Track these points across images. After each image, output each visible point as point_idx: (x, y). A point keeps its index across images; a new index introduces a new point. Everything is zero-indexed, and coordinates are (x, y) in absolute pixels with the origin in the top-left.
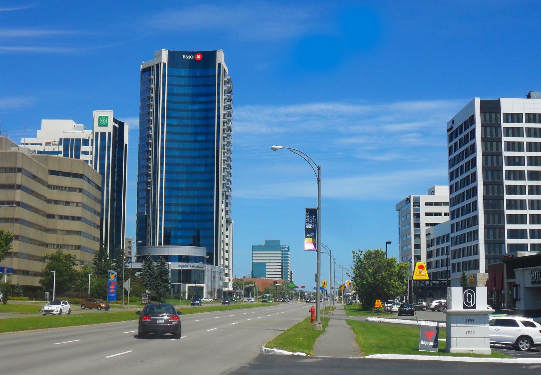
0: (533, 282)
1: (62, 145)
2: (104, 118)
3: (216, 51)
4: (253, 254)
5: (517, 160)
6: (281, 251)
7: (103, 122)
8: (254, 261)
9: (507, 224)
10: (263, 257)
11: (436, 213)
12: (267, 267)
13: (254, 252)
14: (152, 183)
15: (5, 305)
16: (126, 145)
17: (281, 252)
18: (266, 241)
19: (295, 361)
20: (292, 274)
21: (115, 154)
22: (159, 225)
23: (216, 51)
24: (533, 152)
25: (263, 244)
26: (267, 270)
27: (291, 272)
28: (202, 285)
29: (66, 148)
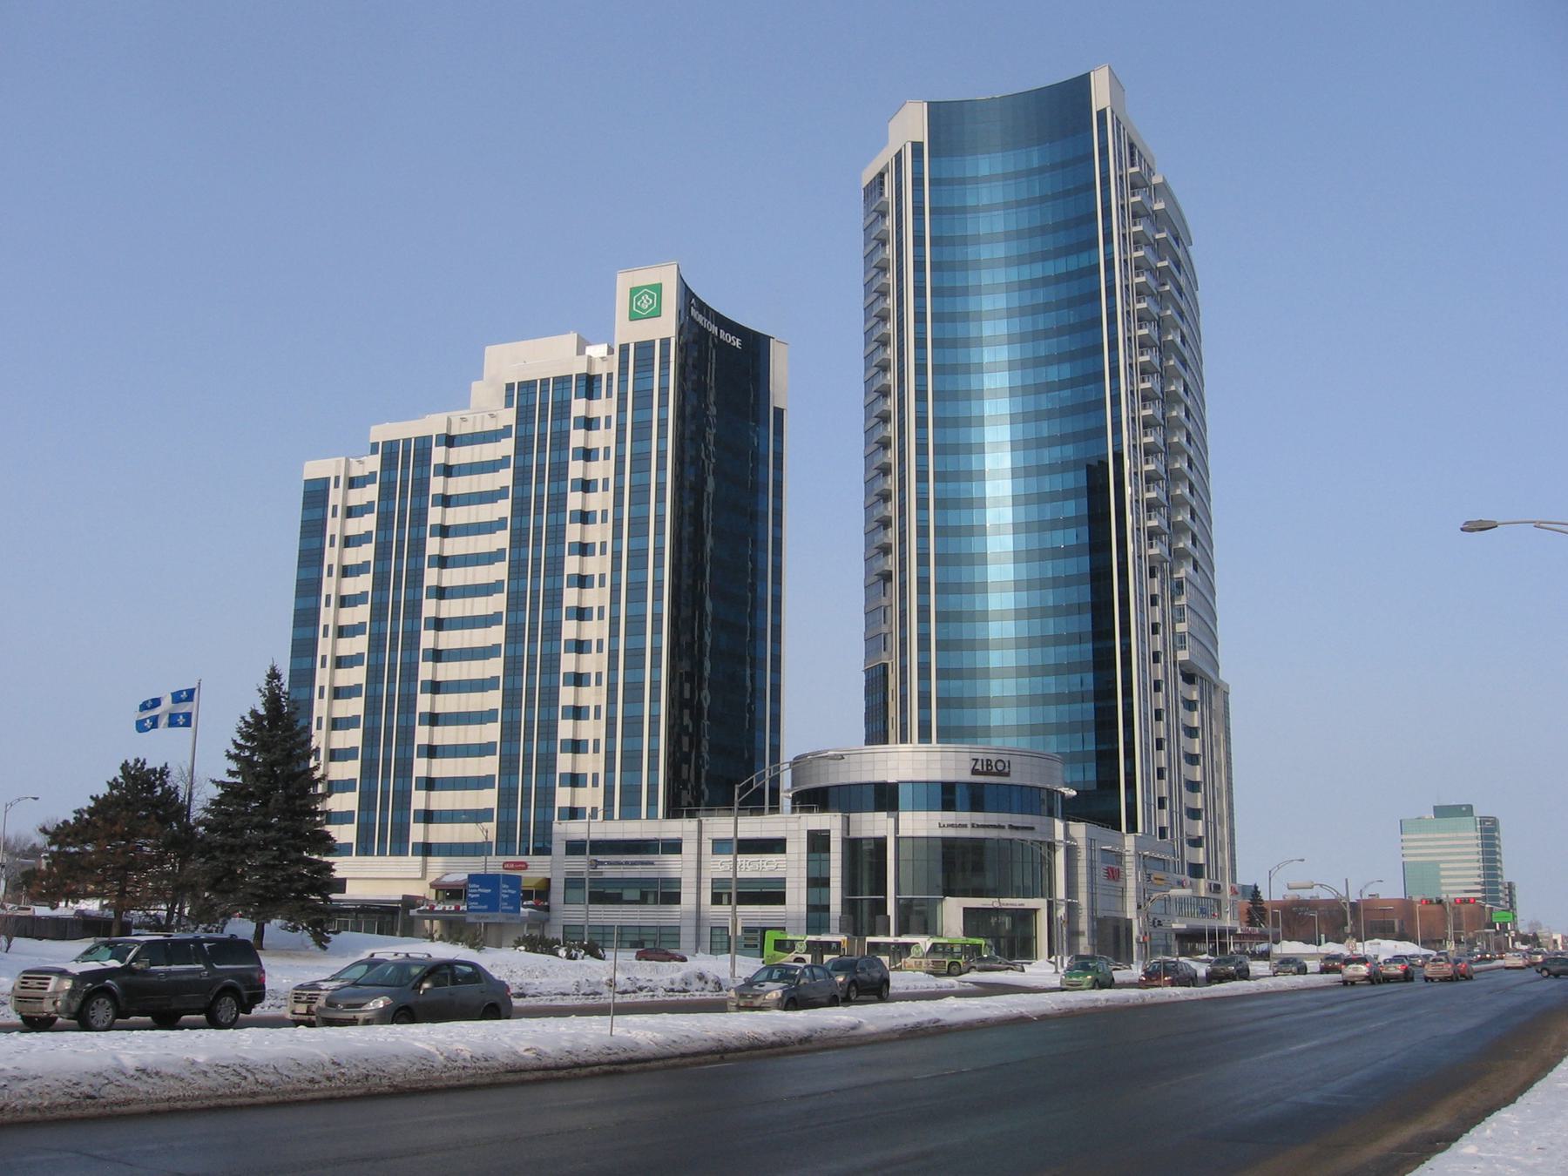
0: (975, 772)
2: (646, 293)
3: (1088, 75)
4: (1403, 848)
5: (788, 945)
7: (644, 304)
8: (1405, 859)
9: (344, 892)
11: (717, 904)
13: (1404, 837)
14: (1153, 746)
15: (407, 952)
18: (1435, 807)
21: (752, 469)
23: (1089, 73)
28: (1029, 903)
29: (524, 416)
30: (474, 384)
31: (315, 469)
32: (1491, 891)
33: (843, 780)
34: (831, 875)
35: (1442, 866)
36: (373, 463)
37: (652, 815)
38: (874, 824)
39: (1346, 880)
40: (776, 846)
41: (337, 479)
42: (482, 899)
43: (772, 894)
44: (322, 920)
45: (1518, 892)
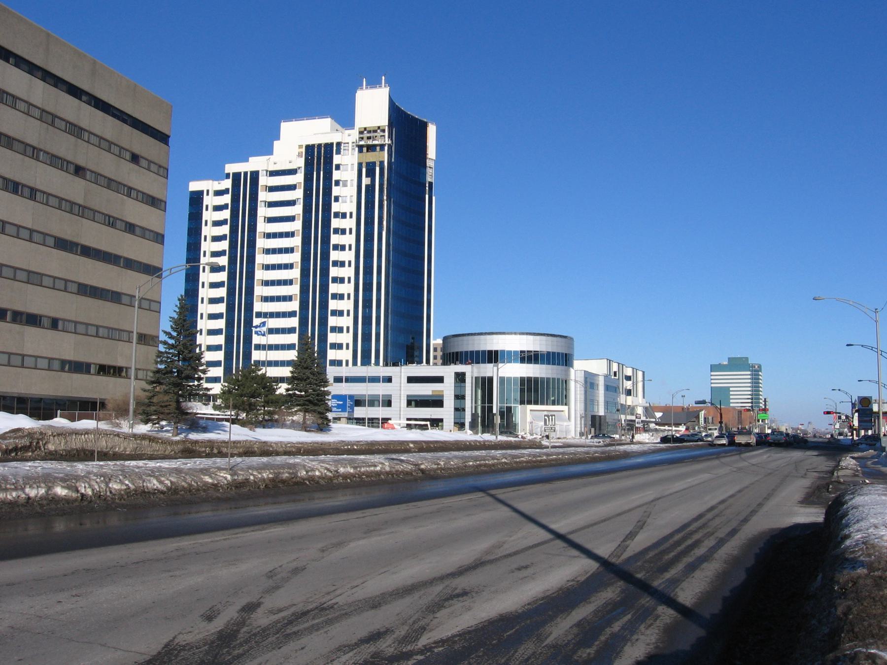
1: (298, 252)
6: (750, 371)
8: (713, 385)
10: (722, 379)
12: (731, 393)
13: (712, 373)
16: (431, 184)
17: (749, 373)
18: (729, 358)
19: (688, 530)
20: (767, 403)
22: (314, 253)
24: (453, 417)
25: (726, 363)
26: (731, 401)
27: (765, 399)
29: (309, 164)
30: (275, 142)
31: (194, 186)
32: (756, 399)
33: (470, 349)
34: (466, 394)
35: (731, 389)
36: (228, 184)
37: (377, 363)
38: (487, 370)
39: (720, 401)
40: (440, 380)
41: (208, 191)
42: (338, 406)
43: (437, 402)
44: (427, 425)
45: (263, 221)
